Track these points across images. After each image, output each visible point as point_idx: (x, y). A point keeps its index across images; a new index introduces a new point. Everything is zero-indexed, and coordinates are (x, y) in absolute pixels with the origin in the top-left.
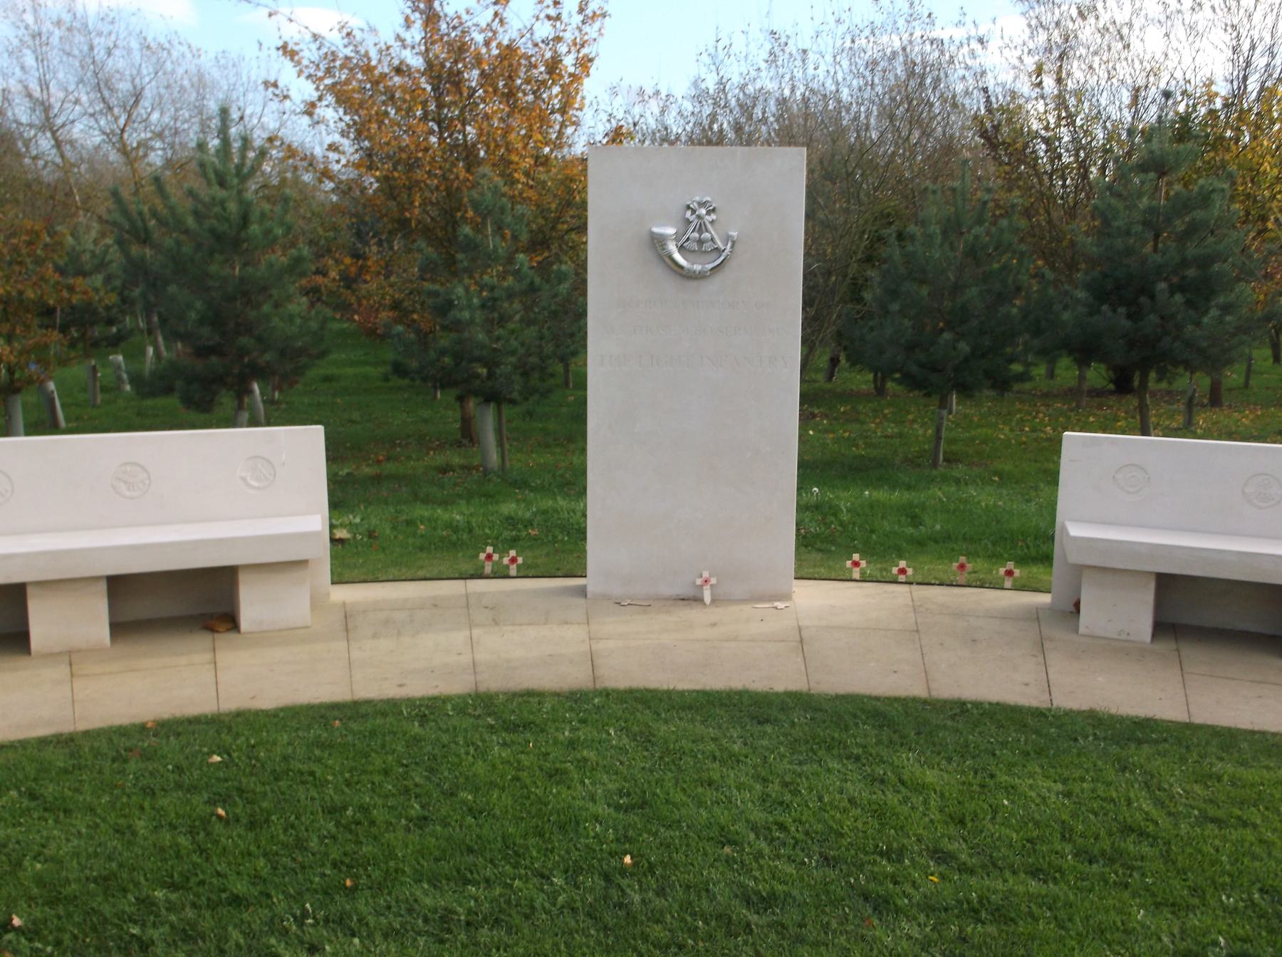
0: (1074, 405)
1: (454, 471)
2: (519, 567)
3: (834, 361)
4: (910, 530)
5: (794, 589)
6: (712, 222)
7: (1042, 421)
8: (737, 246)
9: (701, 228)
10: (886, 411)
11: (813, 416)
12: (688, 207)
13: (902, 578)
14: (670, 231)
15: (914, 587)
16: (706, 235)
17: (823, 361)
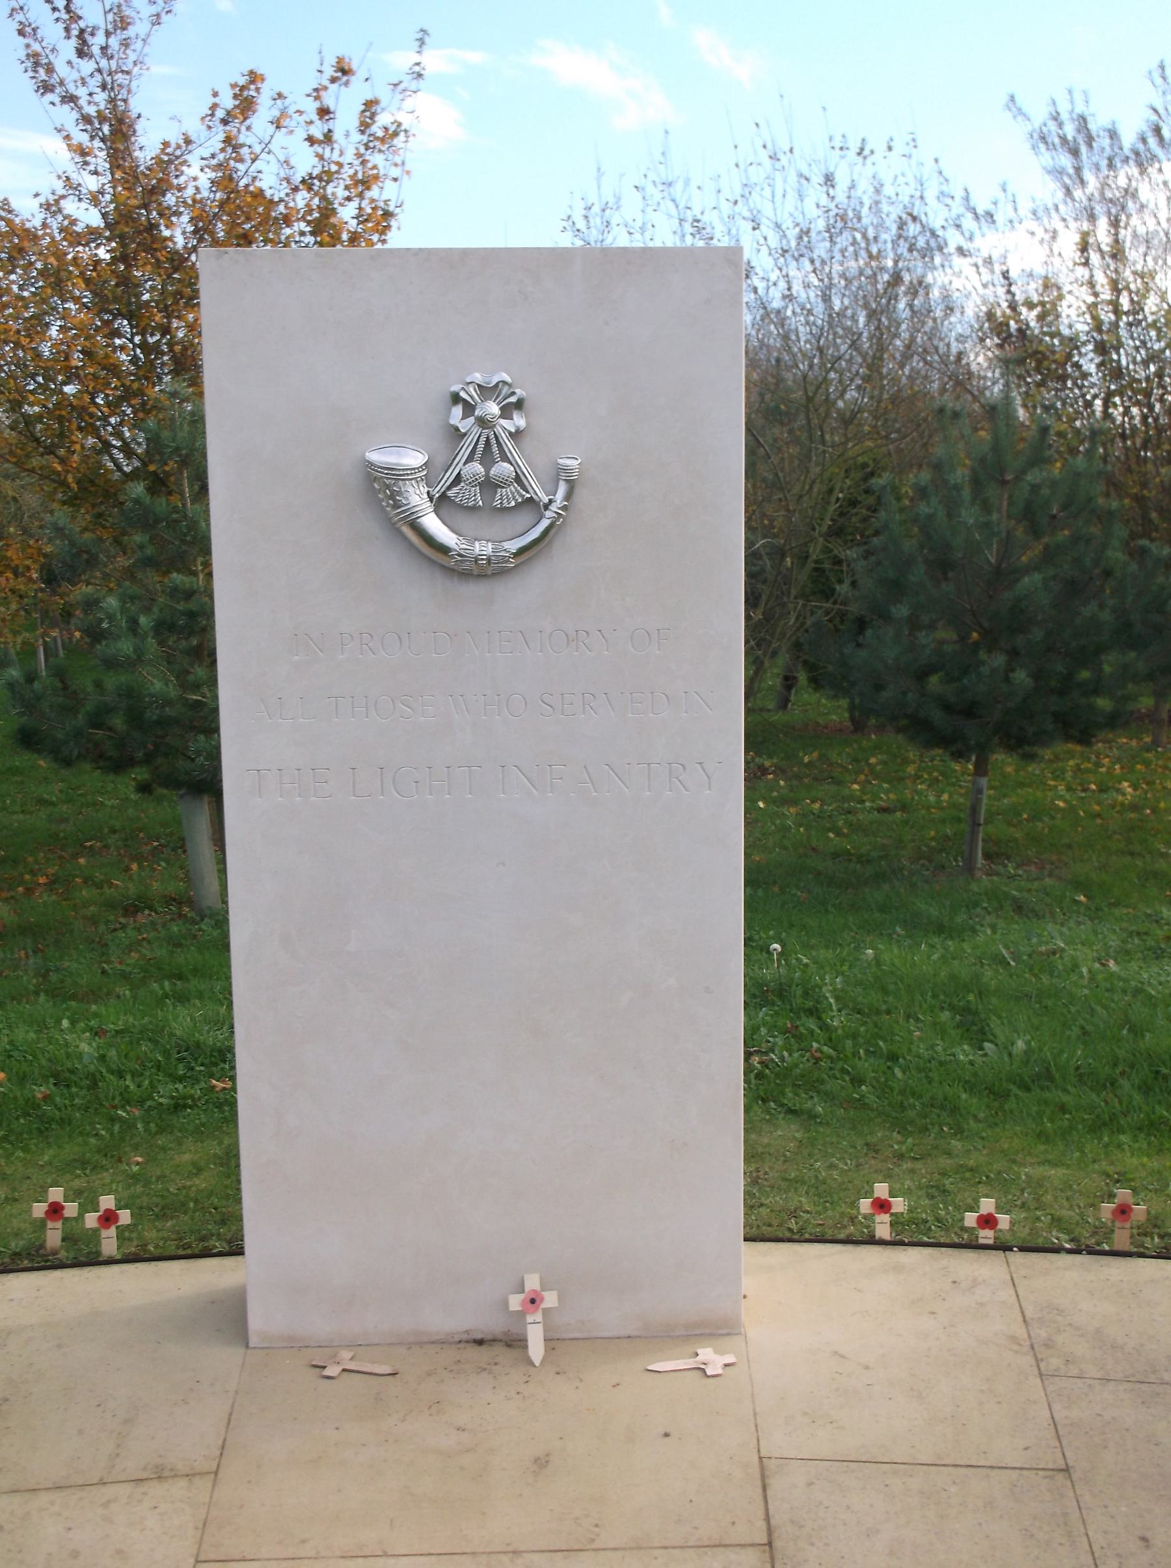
0: (1148, 739)
1: (151, 908)
2: (123, 1235)
3: (789, 682)
4: (964, 1053)
5: (748, 1284)
6: (516, 435)
7: (1110, 770)
8: (581, 493)
9: (489, 452)
10: (873, 760)
11: (764, 771)
12: (456, 399)
13: (986, 1236)
14: (414, 459)
15: (1017, 1257)
16: (503, 469)
17: (772, 680)
